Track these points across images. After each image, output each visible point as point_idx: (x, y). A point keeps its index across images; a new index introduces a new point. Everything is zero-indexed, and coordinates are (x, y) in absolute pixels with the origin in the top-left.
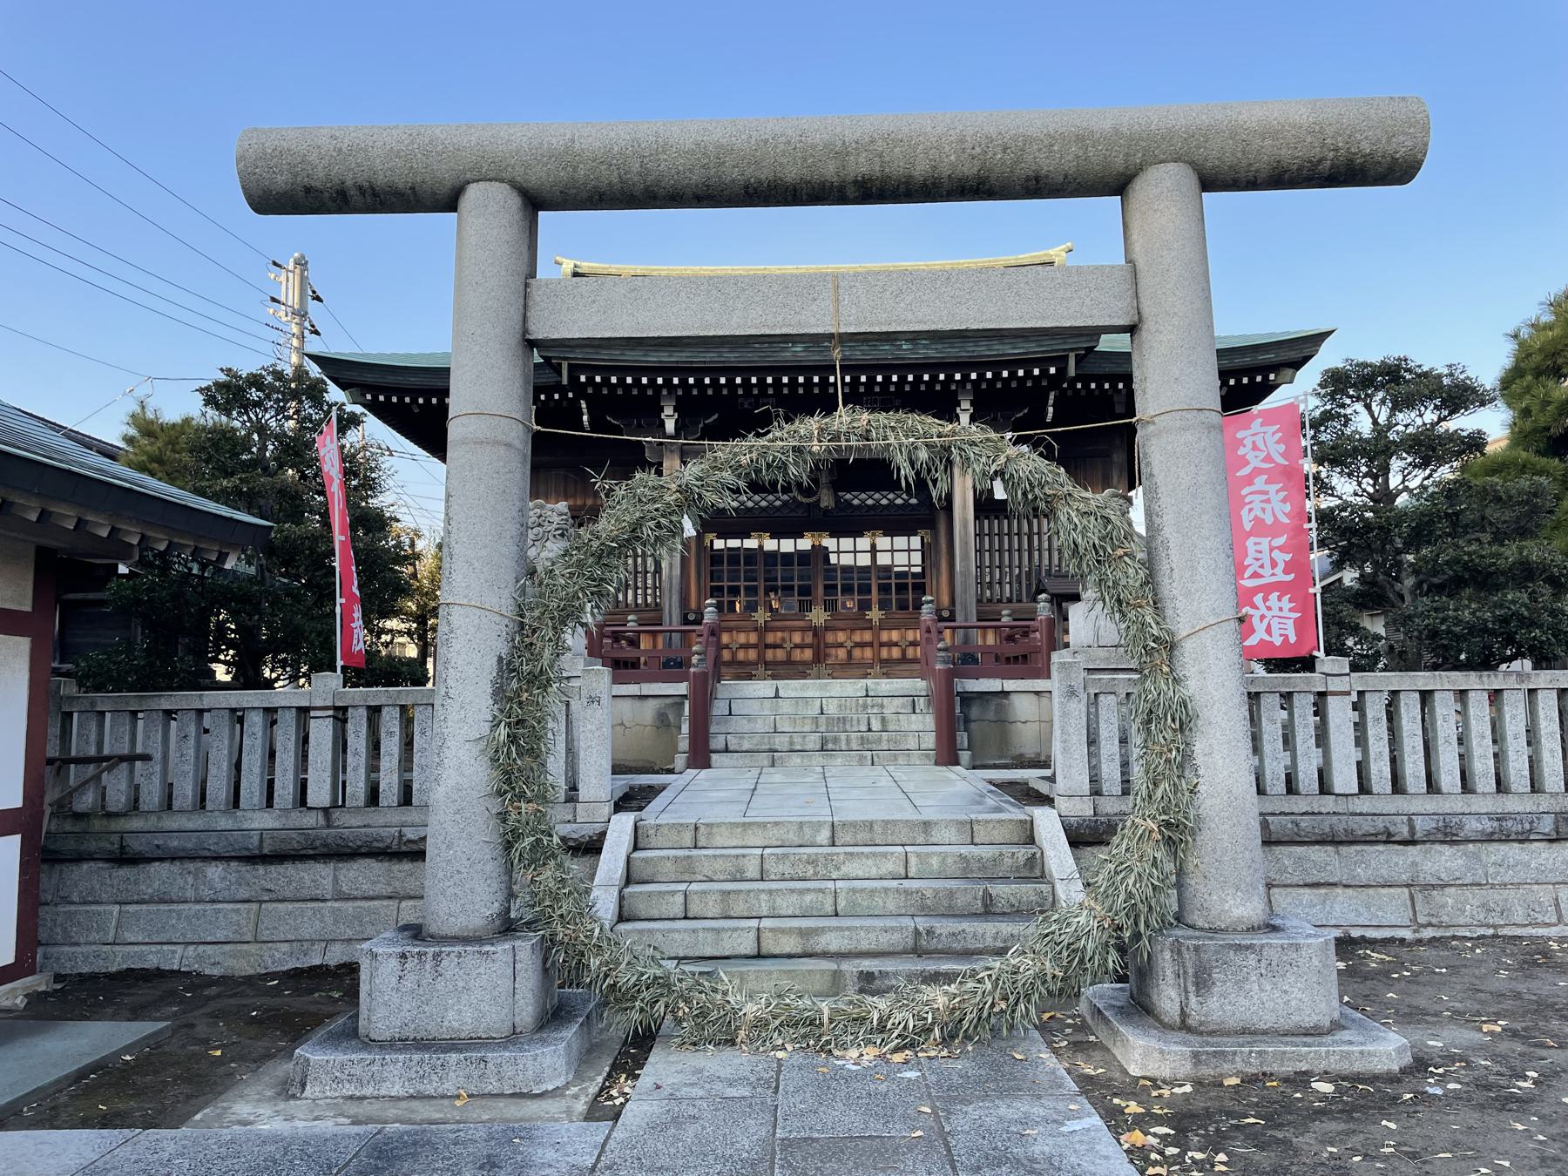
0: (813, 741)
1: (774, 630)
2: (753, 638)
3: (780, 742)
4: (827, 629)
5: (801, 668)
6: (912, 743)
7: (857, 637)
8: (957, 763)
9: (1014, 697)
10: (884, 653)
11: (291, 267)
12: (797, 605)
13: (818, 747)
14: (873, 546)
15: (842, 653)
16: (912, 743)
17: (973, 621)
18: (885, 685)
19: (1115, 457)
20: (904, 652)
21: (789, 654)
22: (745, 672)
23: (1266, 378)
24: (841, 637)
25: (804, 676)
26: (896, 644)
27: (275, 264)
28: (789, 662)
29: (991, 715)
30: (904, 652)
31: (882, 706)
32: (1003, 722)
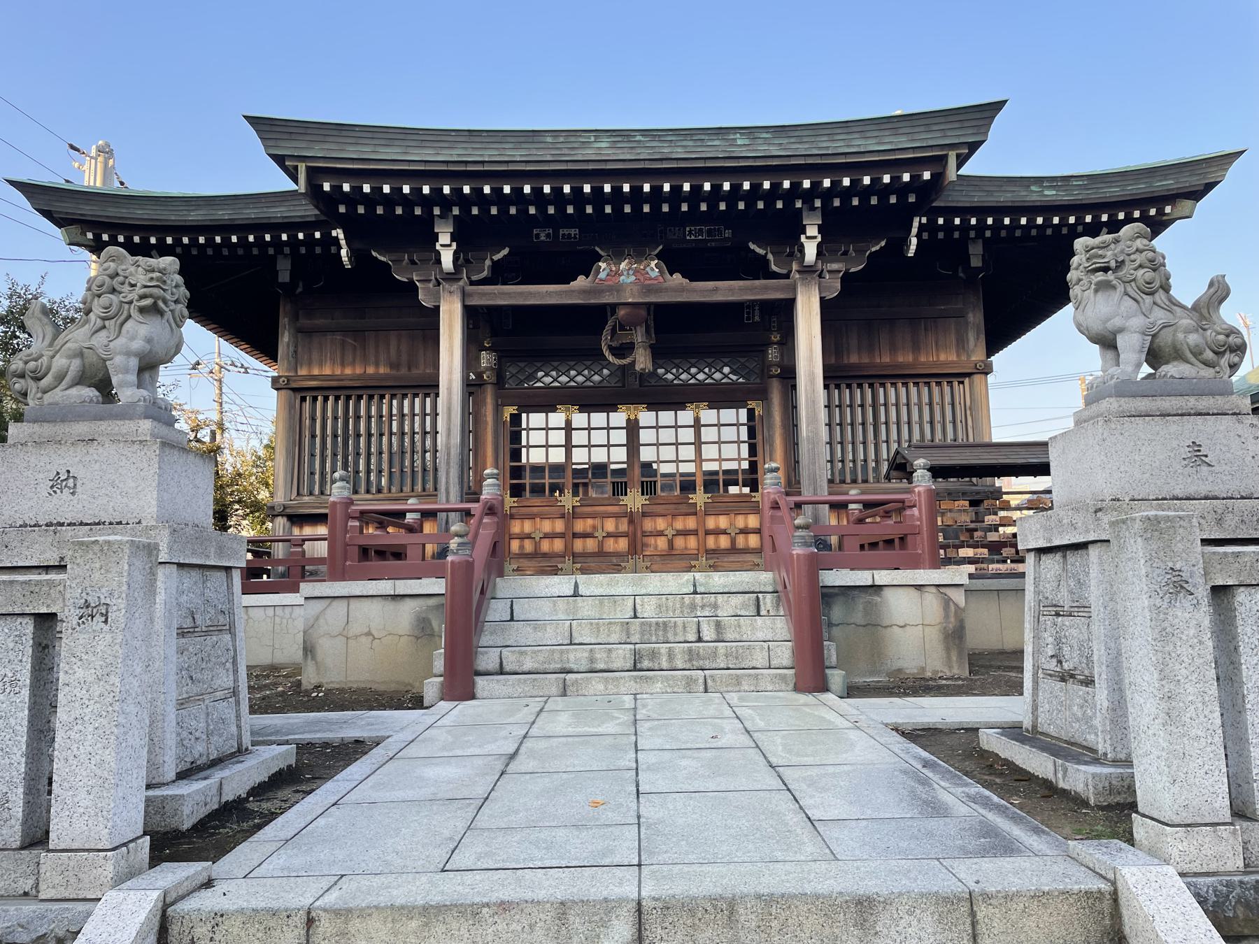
0: (622, 655)
1: (584, 516)
2: (559, 526)
3: (577, 657)
4: (644, 515)
5: (614, 560)
6: (759, 659)
7: (679, 524)
8: (824, 688)
9: (888, 593)
10: (711, 542)
11: (93, 153)
12: (609, 488)
13: (629, 665)
14: (697, 420)
15: (662, 543)
16: (759, 659)
17: (824, 494)
18: (719, 580)
19: (971, 317)
20: (733, 541)
21: (601, 544)
22: (548, 565)
23: (1161, 212)
24: (661, 524)
25: (618, 569)
26: (724, 532)
27: (72, 147)
28: (601, 553)
29: (858, 617)
30: (733, 541)
31: (715, 606)
32: (874, 626)
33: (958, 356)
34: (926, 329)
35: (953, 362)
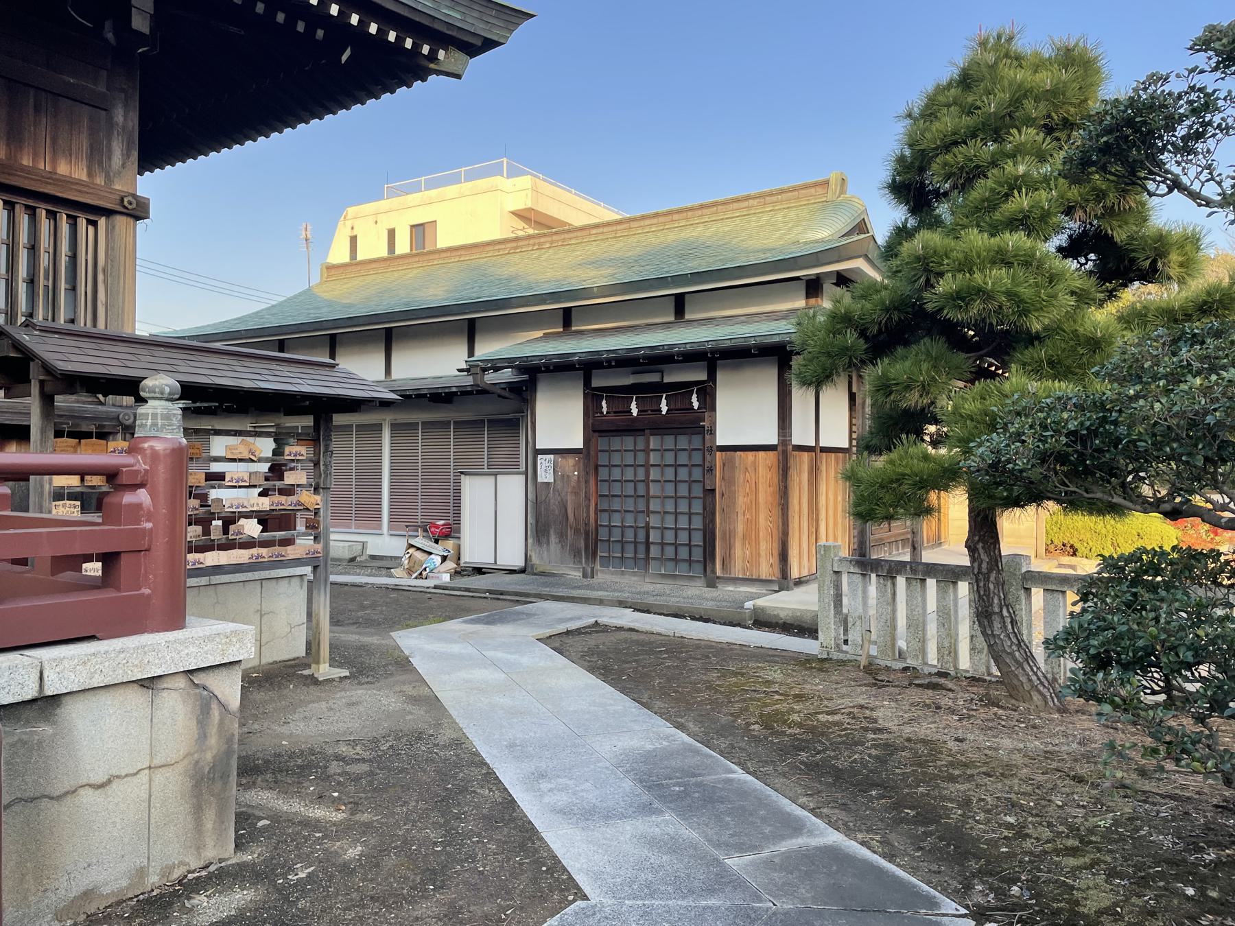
19: (119, 116)
33: (90, 174)
34: (37, 109)
35: (79, 182)
